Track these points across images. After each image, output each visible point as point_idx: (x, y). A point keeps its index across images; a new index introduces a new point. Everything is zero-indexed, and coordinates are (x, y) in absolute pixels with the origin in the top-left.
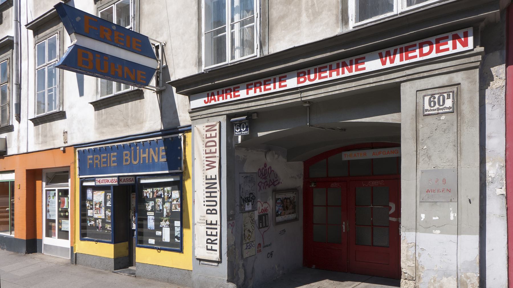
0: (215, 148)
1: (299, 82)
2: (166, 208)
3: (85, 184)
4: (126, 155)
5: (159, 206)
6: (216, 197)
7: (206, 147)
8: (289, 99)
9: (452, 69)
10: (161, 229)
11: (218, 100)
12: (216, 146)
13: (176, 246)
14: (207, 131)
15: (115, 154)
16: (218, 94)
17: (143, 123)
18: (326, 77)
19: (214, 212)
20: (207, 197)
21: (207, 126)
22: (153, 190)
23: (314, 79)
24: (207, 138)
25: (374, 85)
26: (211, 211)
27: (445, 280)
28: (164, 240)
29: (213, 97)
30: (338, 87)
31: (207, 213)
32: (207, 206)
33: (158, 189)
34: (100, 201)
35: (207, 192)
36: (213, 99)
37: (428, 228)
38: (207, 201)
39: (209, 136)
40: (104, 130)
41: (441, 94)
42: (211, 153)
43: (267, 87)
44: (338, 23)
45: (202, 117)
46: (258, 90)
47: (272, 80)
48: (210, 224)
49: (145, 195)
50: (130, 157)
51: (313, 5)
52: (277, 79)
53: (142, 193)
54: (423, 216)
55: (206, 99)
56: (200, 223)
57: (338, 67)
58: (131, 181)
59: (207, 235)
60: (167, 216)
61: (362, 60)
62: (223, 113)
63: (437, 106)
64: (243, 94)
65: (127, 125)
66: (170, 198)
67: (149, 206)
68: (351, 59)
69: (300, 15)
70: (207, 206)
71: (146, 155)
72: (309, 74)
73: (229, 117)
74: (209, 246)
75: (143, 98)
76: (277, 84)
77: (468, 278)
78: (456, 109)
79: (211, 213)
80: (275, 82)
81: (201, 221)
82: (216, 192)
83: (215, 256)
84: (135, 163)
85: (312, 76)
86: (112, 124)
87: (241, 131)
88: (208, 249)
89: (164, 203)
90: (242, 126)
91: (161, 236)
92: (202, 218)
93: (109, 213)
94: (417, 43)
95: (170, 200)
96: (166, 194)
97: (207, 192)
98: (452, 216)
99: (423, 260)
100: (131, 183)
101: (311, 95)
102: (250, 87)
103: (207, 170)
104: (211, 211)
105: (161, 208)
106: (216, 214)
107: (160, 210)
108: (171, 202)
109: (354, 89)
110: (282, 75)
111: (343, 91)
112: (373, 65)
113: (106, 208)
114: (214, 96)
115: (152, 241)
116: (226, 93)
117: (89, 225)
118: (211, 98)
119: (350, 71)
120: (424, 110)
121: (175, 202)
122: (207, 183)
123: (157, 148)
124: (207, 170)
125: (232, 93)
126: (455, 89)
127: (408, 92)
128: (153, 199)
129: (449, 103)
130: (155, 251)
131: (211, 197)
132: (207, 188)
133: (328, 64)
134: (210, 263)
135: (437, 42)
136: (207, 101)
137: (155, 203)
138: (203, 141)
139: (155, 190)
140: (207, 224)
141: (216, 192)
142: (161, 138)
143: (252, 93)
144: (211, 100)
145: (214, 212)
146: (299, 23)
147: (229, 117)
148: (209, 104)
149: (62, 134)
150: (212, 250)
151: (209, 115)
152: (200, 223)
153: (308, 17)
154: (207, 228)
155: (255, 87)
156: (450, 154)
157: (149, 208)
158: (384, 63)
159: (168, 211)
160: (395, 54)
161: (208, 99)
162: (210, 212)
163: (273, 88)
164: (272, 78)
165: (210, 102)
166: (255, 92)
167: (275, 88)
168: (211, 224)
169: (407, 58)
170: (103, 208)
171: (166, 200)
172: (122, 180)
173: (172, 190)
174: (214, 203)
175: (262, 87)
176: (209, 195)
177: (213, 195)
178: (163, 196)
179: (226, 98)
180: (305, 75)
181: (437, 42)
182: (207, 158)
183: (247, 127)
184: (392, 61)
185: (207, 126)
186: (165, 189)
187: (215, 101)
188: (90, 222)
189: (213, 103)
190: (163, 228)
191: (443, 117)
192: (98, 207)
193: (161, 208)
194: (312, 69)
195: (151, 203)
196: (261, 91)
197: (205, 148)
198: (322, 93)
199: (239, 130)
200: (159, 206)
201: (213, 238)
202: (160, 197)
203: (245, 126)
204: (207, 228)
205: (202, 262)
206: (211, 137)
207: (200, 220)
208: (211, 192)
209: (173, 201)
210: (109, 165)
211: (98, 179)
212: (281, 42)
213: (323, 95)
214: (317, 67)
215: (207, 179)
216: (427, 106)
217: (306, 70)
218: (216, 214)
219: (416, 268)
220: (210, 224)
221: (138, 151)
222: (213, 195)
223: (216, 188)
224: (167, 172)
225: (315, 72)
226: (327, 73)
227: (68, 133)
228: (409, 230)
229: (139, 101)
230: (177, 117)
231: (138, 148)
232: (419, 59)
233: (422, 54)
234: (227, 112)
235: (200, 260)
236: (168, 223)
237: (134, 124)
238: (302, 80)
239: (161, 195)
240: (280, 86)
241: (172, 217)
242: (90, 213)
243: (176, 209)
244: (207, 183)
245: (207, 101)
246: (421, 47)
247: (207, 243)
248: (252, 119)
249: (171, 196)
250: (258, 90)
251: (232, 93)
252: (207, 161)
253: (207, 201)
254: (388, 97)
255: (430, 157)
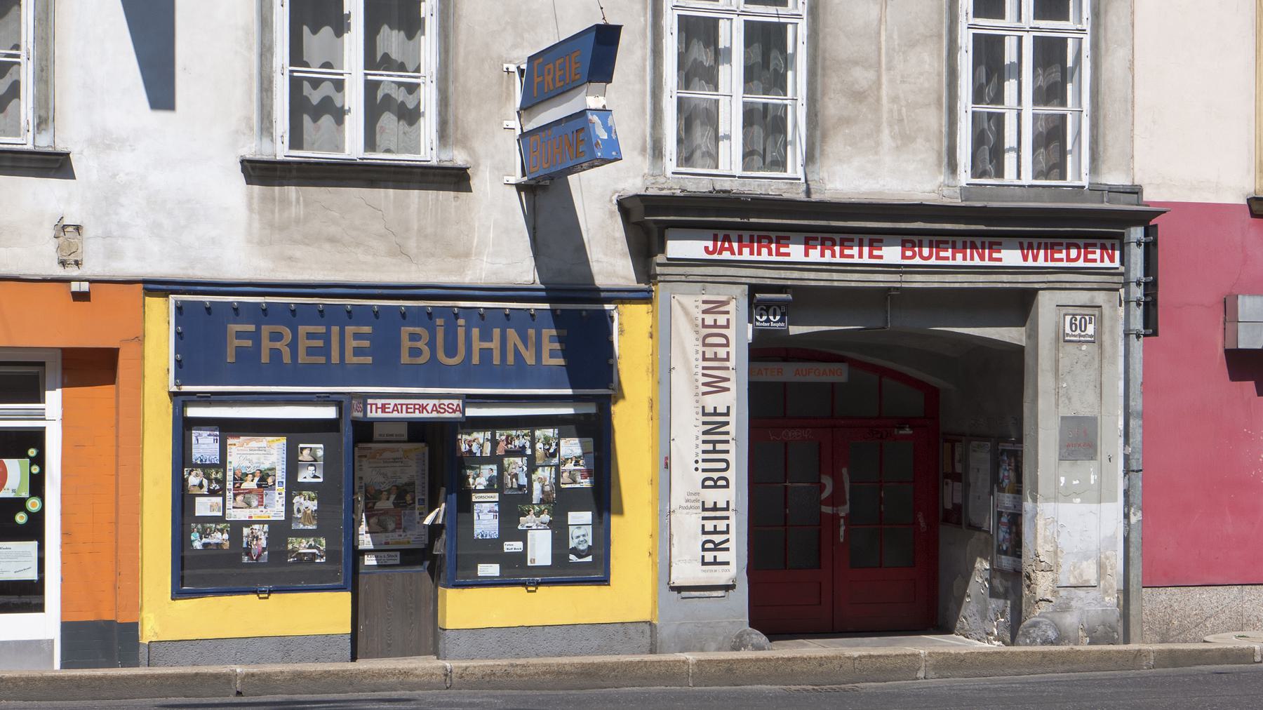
0: (727, 349)
1: (904, 257)
2: (541, 480)
3: (193, 412)
4: (414, 337)
5: (516, 476)
6: (727, 452)
7: (704, 345)
8: (881, 280)
9: (1095, 286)
10: (522, 536)
11: (740, 253)
12: (727, 345)
13: (593, 569)
14: (704, 312)
15: (367, 329)
16: (740, 240)
17: (467, 255)
18: (947, 258)
19: (722, 483)
20: (704, 452)
21: (704, 302)
22: (493, 435)
23: (925, 256)
24: (704, 326)
25: (1008, 285)
26: (715, 482)
27: (1085, 563)
28: (533, 560)
29: (726, 245)
30: (960, 278)
31: (704, 487)
32: (704, 470)
33: (513, 433)
34: (266, 465)
35: (704, 442)
36: (726, 249)
37: (1065, 495)
38: (704, 461)
39: (709, 321)
40: (298, 252)
41: (1083, 316)
42: (716, 359)
43: (847, 252)
44: (940, 165)
45: (691, 278)
46: (828, 253)
47: (857, 241)
48: (713, 511)
49: (464, 447)
50: (432, 344)
51: (901, 121)
52: (866, 241)
53: (455, 443)
54: (1063, 480)
55: (710, 244)
56: (686, 508)
57: (965, 247)
58: (454, 411)
59: (704, 533)
60: (542, 501)
61: (995, 246)
62: (744, 280)
63: (1078, 331)
64: (796, 252)
65: (400, 252)
66: (553, 455)
67: (480, 478)
68: (984, 239)
69: (878, 129)
70: (704, 470)
71: (494, 345)
72: (921, 246)
73: (754, 289)
74: (709, 557)
75: (469, 190)
76: (866, 250)
77: (1107, 558)
78: (1097, 340)
79: (716, 486)
80: (861, 245)
81: (689, 504)
82: (727, 442)
83: (721, 576)
84: (451, 361)
85: (926, 251)
86: (332, 240)
87: (768, 321)
88: (704, 563)
89: (532, 468)
90: (771, 311)
91: (523, 555)
92: (693, 498)
93: (306, 503)
94: (1065, 241)
95: (555, 461)
96: (539, 445)
97: (704, 442)
98: (1093, 478)
99: (1063, 541)
100: (453, 415)
101: (918, 281)
102: (811, 243)
103: (704, 394)
104: (715, 482)
105: (523, 480)
106: (727, 486)
107: (521, 487)
108: (557, 467)
109: (981, 285)
110: (876, 239)
111: (966, 285)
112: (1011, 257)
113: (293, 488)
114: (730, 242)
115: (489, 570)
116: (759, 242)
117: (198, 545)
118: (722, 246)
119: (982, 258)
120: (1065, 334)
121: (570, 466)
122: (704, 423)
123: (531, 332)
124: (704, 394)
125: (773, 246)
126: (1096, 311)
127: (1046, 304)
128: (494, 459)
129: (1090, 329)
130: (522, 590)
131: (714, 451)
132: (704, 433)
133: (950, 239)
134: (707, 594)
135: (1086, 246)
136: (711, 249)
137: (501, 469)
138: (697, 332)
139: (501, 435)
140: (704, 509)
141: (727, 442)
142: (546, 306)
143: (815, 255)
144: (723, 249)
145: (722, 483)
146: (878, 144)
147: (754, 289)
148: (715, 257)
149: (49, 232)
150: (715, 563)
151: (709, 279)
152: (686, 508)
153: (893, 137)
154: (704, 518)
155: (822, 244)
156: (1091, 397)
157: (481, 482)
158: (1025, 259)
159: (547, 488)
160: (1038, 249)
161: (715, 246)
162: (712, 483)
163: (857, 255)
164: (856, 237)
165: (720, 253)
166: (822, 255)
167: (861, 256)
168: (715, 508)
169: (1053, 260)
170: (281, 489)
171: (539, 462)
172: (429, 408)
173: (562, 435)
174: (723, 465)
175: (837, 249)
176: (710, 447)
177: (719, 447)
178: (529, 452)
179: (759, 253)
180: (914, 246)
181: (1086, 246)
182: (704, 368)
183: (783, 315)
184: (1035, 259)
185: (704, 302)
186: (538, 433)
187: (733, 253)
188: (204, 533)
189: (726, 255)
190: (530, 533)
191: (1084, 347)
192: (250, 484)
193: (523, 480)
194: (926, 239)
195: (488, 471)
196: (833, 255)
197: (701, 349)
198: (934, 281)
199: (764, 318)
200: (516, 476)
201: (717, 538)
202: (520, 452)
203: (778, 311)
204: (704, 518)
205: (685, 594)
206: (715, 326)
207: (687, 501)
208: (714, 442)
209: (565, 462)
210: (335, 358)
211: (380, 402)
212: (845, 166)
213: (936, 285)
214: (935, 239)
215: (704, 414)
216: (1068, 330)
217: (916, 239)
218: (727, 486)
219: (1056, 553)
220: (713, 511)
221: (461, 332)
222: (719, 447)
223: (727, 433)
224: (569, 392)
225: (931, 247)
226: (949, 253)
227: (88, 231)
228: (1047, 500)
229: (452, 193)
230: (585, 262)
231: (461, 322)
232: (1065, 264)
233: (1069, 260)
234: (754, 281)
235: (679, 589)
236: (546, 518)
237: (433, 255)
238: (909, 253)
239: (524, 447)
240: (871, 256)
241: (561, 503)
242: (205, 506)
243: (575, 482)
244: (704, 423)
245: (711, 249)
246: (1068, 248)
247: (704, 549)
248: (804, 300)
249: (557, 450)
250: (828, 253)
251: (773, 246)
252: (704, 375)
253: (704, 461)
254: (1017, 304)
255: (1069, 399)
